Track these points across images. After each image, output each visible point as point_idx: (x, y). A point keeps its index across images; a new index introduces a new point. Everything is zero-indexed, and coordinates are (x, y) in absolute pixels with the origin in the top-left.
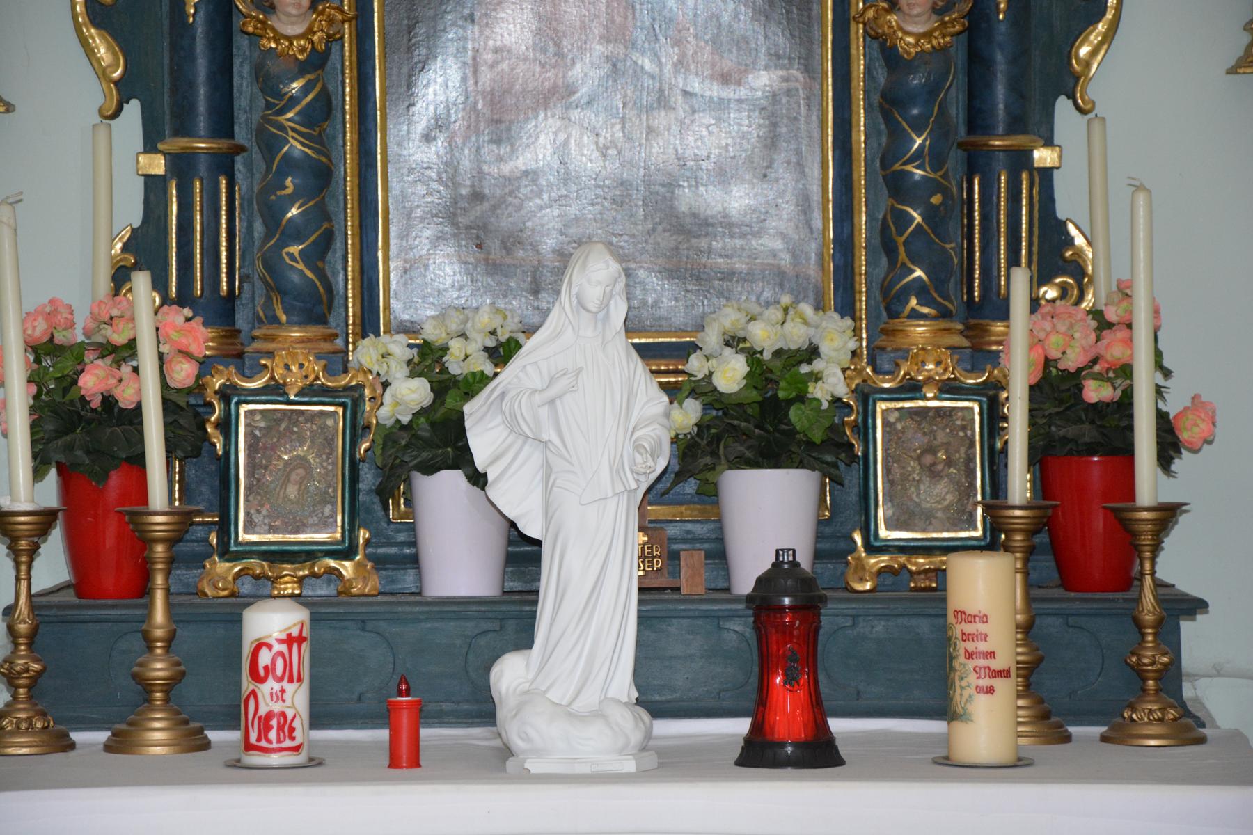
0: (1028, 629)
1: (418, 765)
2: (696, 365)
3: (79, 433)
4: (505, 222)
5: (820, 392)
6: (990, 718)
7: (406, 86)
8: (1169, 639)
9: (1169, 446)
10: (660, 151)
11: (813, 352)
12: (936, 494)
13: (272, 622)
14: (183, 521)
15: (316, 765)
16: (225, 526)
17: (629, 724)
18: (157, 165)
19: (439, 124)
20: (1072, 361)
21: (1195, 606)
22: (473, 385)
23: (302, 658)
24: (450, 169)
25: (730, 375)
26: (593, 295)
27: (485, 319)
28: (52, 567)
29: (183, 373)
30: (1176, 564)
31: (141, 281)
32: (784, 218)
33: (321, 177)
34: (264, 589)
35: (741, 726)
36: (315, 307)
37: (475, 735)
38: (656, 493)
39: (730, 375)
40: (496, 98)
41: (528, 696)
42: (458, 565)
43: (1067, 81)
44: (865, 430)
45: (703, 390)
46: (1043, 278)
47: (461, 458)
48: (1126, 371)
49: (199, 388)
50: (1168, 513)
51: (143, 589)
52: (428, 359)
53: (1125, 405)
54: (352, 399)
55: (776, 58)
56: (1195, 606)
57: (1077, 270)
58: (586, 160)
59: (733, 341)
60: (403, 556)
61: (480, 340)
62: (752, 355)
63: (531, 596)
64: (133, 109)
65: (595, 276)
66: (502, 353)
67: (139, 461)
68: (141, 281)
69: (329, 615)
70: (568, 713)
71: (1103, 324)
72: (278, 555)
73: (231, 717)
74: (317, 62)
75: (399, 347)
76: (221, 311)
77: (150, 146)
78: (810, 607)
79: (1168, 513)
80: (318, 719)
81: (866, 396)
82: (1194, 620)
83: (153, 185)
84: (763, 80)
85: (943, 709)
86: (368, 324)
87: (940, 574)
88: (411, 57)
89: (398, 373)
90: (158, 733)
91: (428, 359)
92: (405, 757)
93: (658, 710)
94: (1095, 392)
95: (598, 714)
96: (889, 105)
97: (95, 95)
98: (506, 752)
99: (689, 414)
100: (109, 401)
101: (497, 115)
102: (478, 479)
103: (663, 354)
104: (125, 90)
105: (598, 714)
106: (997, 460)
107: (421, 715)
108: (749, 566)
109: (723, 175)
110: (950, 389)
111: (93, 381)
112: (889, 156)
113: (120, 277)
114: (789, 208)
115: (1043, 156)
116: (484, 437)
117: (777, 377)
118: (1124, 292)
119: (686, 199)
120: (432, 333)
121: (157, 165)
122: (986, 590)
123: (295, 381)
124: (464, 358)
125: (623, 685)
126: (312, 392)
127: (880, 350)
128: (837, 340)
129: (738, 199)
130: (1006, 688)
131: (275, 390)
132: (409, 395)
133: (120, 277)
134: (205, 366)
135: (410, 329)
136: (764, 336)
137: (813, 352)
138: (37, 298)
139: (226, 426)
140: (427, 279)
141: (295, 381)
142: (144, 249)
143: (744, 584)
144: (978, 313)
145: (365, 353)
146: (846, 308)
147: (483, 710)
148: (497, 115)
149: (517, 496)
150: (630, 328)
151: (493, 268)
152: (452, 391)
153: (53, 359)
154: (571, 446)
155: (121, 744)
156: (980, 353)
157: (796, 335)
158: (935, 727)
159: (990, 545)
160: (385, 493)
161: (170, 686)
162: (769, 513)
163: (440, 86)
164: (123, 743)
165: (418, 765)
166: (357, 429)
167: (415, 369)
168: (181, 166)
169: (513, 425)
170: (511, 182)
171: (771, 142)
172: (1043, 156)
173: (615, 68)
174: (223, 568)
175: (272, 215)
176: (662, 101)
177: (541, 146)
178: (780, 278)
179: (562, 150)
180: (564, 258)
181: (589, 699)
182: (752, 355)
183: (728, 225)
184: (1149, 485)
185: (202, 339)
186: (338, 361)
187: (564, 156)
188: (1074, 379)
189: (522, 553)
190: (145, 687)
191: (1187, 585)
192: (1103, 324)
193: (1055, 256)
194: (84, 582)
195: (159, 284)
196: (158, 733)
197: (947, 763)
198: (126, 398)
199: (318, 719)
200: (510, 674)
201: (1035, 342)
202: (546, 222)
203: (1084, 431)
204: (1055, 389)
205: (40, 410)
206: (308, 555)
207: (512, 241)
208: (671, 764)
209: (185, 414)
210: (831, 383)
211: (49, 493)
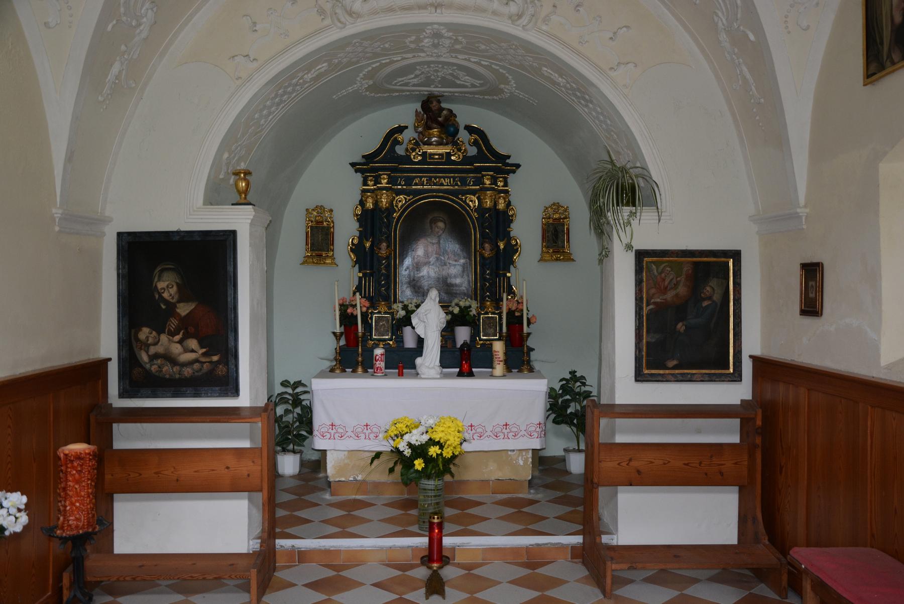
0: (506, 354)
1: (804, 266)
2: (450, 309)
3: (347, 319)
4: (419, 284)
5: (471, 313)
6: (499, 369)
7: (402, 262)
8: (529, 355)
9: (529, 323)
10: (444, 273)
11: (470, 307)
12: (491, 331)
13: (379, 352)
14: (364, 334)
15: (386, 376)
16: (371, 335)
17: (439, 369)
18: (361, 275)
19: (408, 268)
20: (514, 308)
21: (533, 350)
22: (413, 311)
23: (383, 358)
24: (409, 275)
25: (456, 310)
26: (433, 297)
27: (415, 301)
28: (343, 342)
29: (364, 309)
30: (530, 343)
31: (358, 294)
32: (465, 284)
33: (388, 277)
34: (377, 346)
35: (458, 370)
36: (387, 299)
37: (413, 371)
38: (443, 330)
39: (456, 310)
40: (417, 264)
41: (421, 365)
42: (410, 343)
43: (512, 262)
44: (479, 320)
45: (452, 313)
46: (508, 295)
47: (410, 324)
48: (522, 310)
49: (367, 312)
50: (529, 334)
51: (358, 346)
52: (405, 307)
53: (522, 316)
54: (392, 314)
55: (464, 258)
56: (533, 350)
57: (514, 293)
58: (432, 274)
59: (457, 305)
60: (400, 340)
61: (414, 304)
62: (460, 307)
63: (422, 347)
64: (357, 266)
65: (434, 294)
66: (418, 306)
67: (357, 324)
68: (358, 294)
69: (388, 350)
70: (428, 367)
71: (518, 303)
72: (380, 340)
73: (372, 368)
74: (388, 258)
75: (400, 305)
76: (370, 299)
77: (360, 272)
78: (469, 350)
79: (529, 334)
80: (386, 368)
81: (479, 314)
82: (742, 401)
83: (360, 278)
84: (462, 261)
85: (492, 367)
86: (395, 302)
87: (491, 344)
88: (402, 258)
89: (400, 310)
90: (360, 369)
91: (405, 307)
92: (401, 374)
93: (443, 368)
94: (517, 314)
95: (433, 368)
96: (483, 266)
97: (350, 264)
98: (418, 374)
99: (449, 317)
100: (352, 314)
101: (417, 267)
102: (413, 328)
103: (445, 306)
104: (356, 262)
105: (433, 368)
106: (501, 325)
107: (404, 368)
108: (459, 343)
109: (455, 277)
110: (493, 313)
111: (349, 311)
112: (483, 273)
113: (354, 293)
114: (466, 282)
115: (508, 275)
116: (414, 321)
117: (465, 310)
118: (522, 297)
119: (449, 281)
120: (406, 303)
121: (361, 275)
122: (499, 347)
123: (383, 311)
124: (411, 307)
125: (438, 363)
126: (385, 313)
127: (482, 306)
128: (474, 305)
129: (458, 281)
130: (502, 363)
131: (379, 313)
132: (402, 313)
133: (354, 293)
134: (368, 308)
135: (402, 302)
136: (462, 304)
137: (470, 307)
138: (341, 297)
139: (371, 318)
140: (405, 293)
141: (383, 311)
142: (358, 289)
143: (458, 346)
144: (497, 302)
145: (395, 306)
146: (476, 299)
147: (414, 367)
148: (417, 267)
149: (420, 331)
150: (440, 302)
151: (416, 292)
152: (409, 312)
153: (343, 307)
154: (429, 321)
155: (354, 371)
156: (498, 307)
157: (467, 304)
158: (490, 370)
159: (499, 340)
160: (398, 330)
161: (362, 362)
162: (463, 334)
163: (408, 262)
164: (354, 371)
165: (804, 266)
166: (393, 319)
167: (403, 309)
168: (365, 275)
169: (419, 319)
170: (419, 278)
171: (463, 271)
172: (508, 275)
173: (437, 259)
174: (371, 342)
175: (380, 283)
176: (445, 264)
177: (424, 272)
178: (465, 294)
179: (428, 272)
180: (428, 290)
181: (432, 365)
182: (460, 307)
183: (456, 285)
184: (526, 329)
185: (367, 304)
186: (390, 308)
187: (428, 273)
188: (514, 312)
189: (420, 341)
190: (358, 363)
191: (532, 346)
192: (518, 303)
193: (510, 291)
194: (348, 344)
195: (361, 294)
196: (360, 369)
197: (492, 376)
198: (355, 313)
199: (386, 368)
200: (418, 361)
201: (507, 305)
202: (425, 284)
203: (515, 320)
204: (510, 313)
205: (341, 315)
206: (385, 340)
207: (420, 287)
208: (446, 376)
209: (364, 316)
210: (474, 312)
211: (342, 329)
